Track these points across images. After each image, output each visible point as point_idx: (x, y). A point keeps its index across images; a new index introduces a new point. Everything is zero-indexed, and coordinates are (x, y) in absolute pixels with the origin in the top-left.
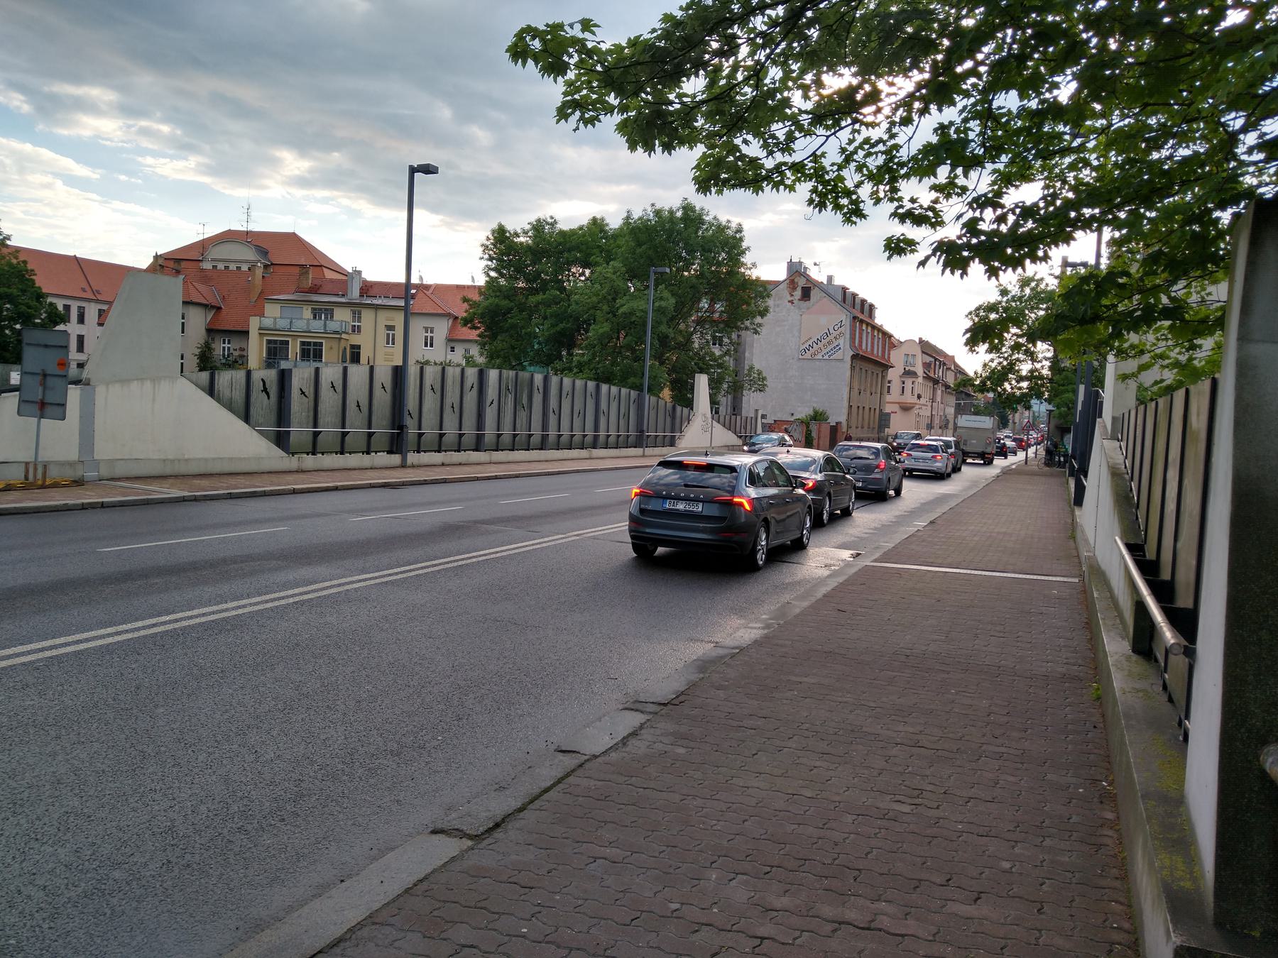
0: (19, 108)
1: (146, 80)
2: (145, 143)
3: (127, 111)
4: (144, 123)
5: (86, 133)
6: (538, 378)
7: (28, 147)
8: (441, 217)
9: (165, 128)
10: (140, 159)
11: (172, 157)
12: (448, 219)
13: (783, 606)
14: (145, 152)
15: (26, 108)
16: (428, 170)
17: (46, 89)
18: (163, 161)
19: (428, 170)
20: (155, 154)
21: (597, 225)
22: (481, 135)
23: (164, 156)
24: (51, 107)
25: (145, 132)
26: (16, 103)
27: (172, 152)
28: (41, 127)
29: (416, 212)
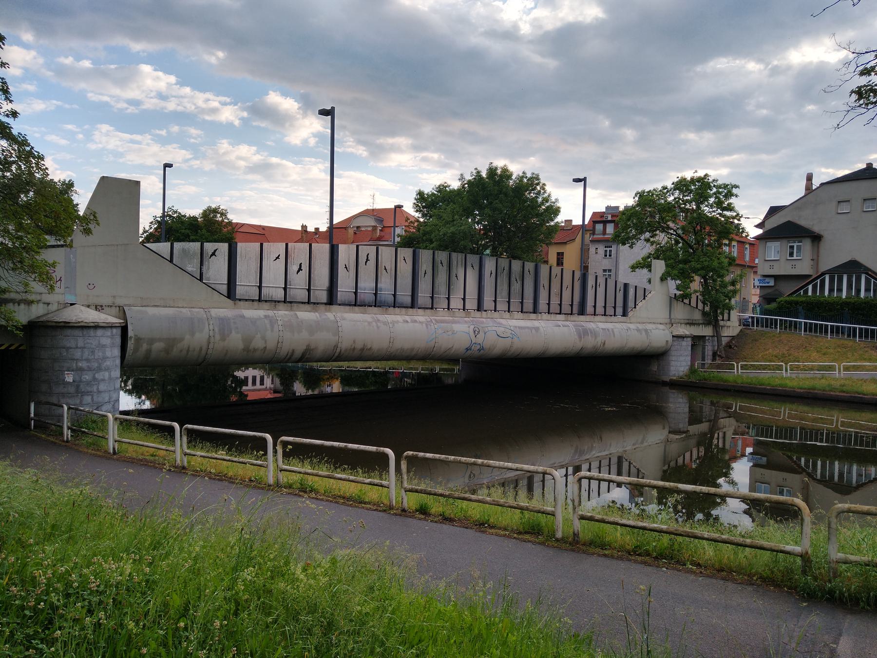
0: (361, 155)
1: (427, 129)
2: (425, 166)
3: (416, 148)
4: (425, 154)
5: (393, 164)
6: (862, 294)
7: (364, 176)
8: (598, 191)
9: (436, 156)
10: (420, 176)
11: (438, 173)
12: (604, 192)
13: (802, 520)
14: (422, 171)
15: (365, 154)
16: (170, 166)
17: (378, 141)
18: (432, 175)
19: (170, 166)
20: (428, 172)
21: (442, 189)
22: (629, 133)
23: (434, 172)
24: (378, 152)
25: (424, 159)
26: (360, 152)
27: (438, 169)
28: (372, 163)
29: (587, 189)
